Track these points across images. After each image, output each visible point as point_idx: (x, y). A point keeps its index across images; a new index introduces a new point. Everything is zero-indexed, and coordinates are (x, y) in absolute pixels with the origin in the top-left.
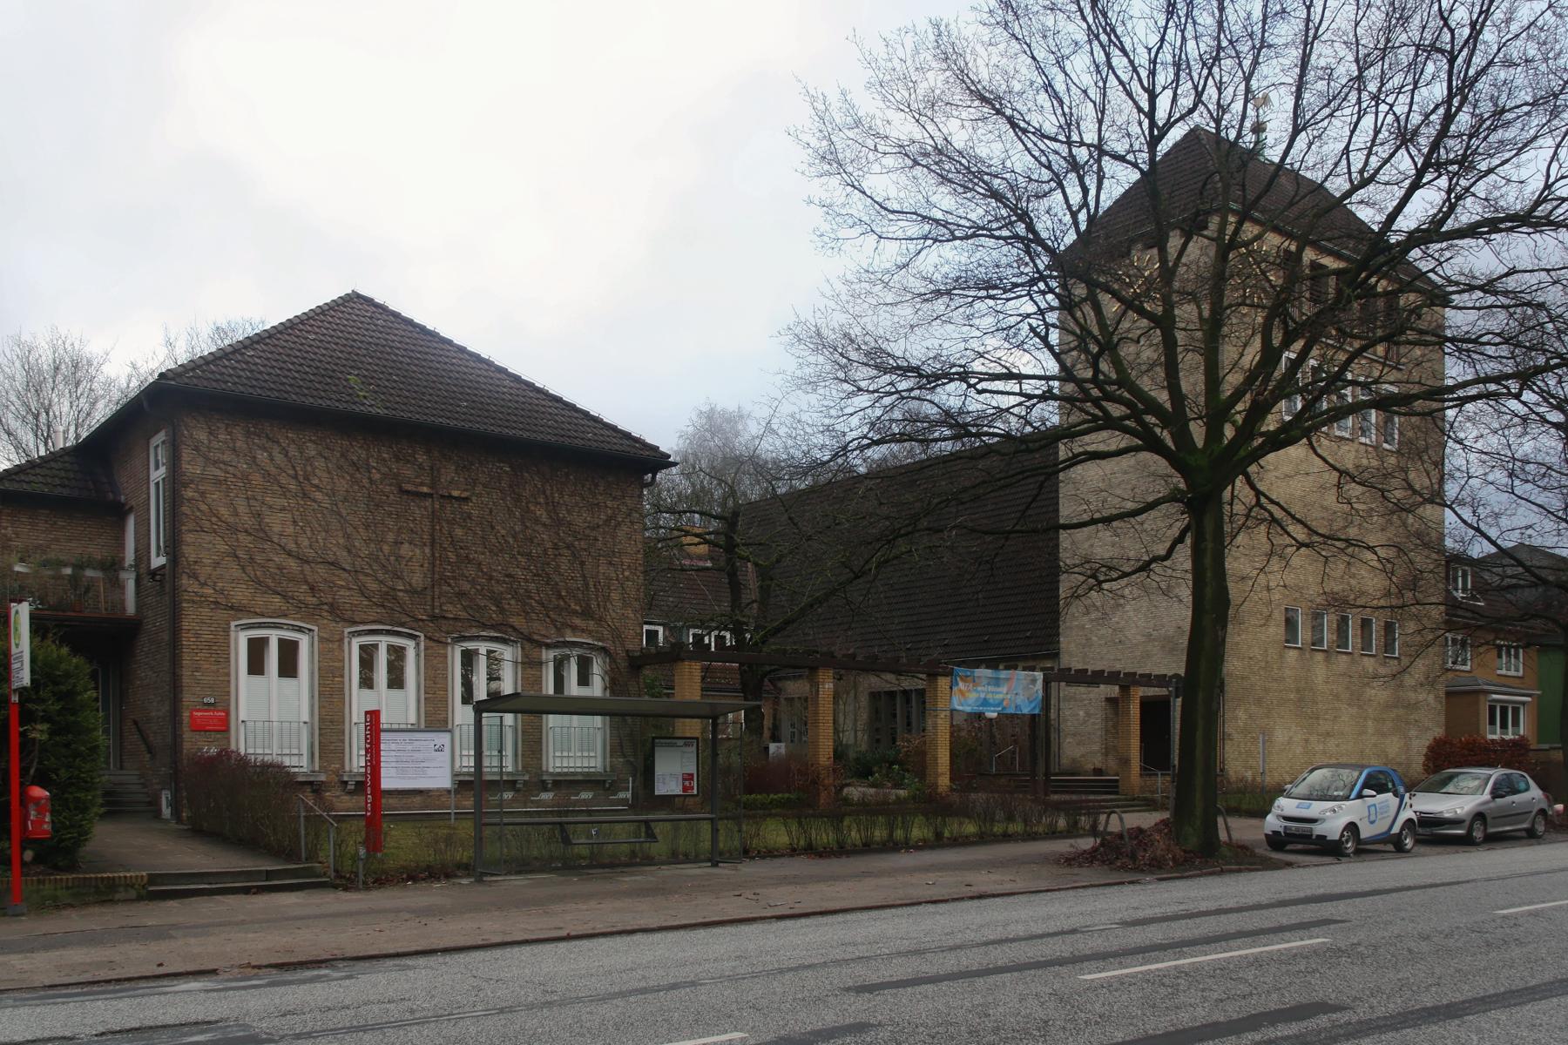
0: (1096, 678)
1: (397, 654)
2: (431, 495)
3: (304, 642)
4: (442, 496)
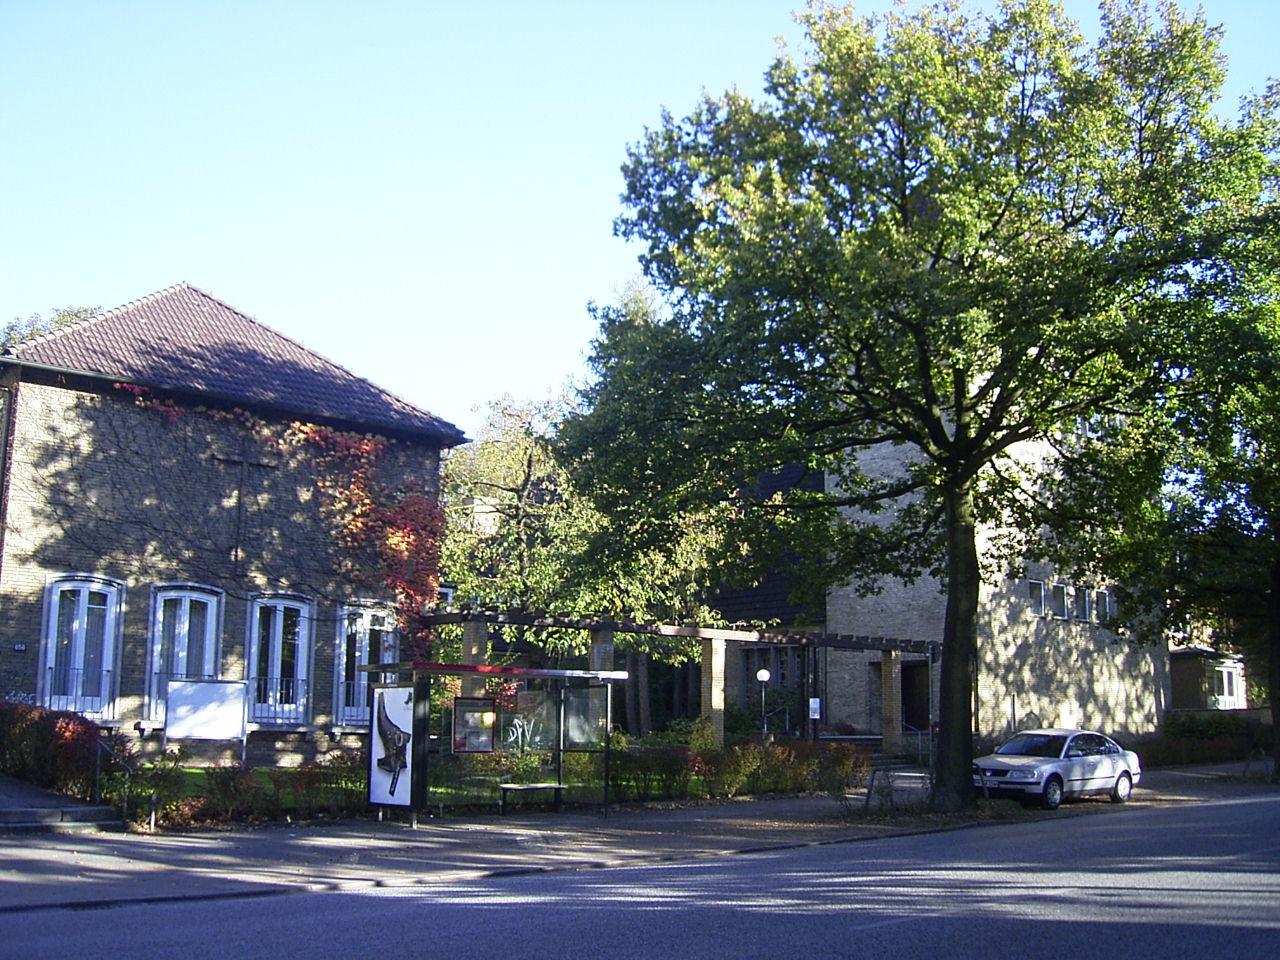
0: (860, 644)
1: (198, 608)
2: (240, 463)
3: (305, 611)
4: (251, 465)
